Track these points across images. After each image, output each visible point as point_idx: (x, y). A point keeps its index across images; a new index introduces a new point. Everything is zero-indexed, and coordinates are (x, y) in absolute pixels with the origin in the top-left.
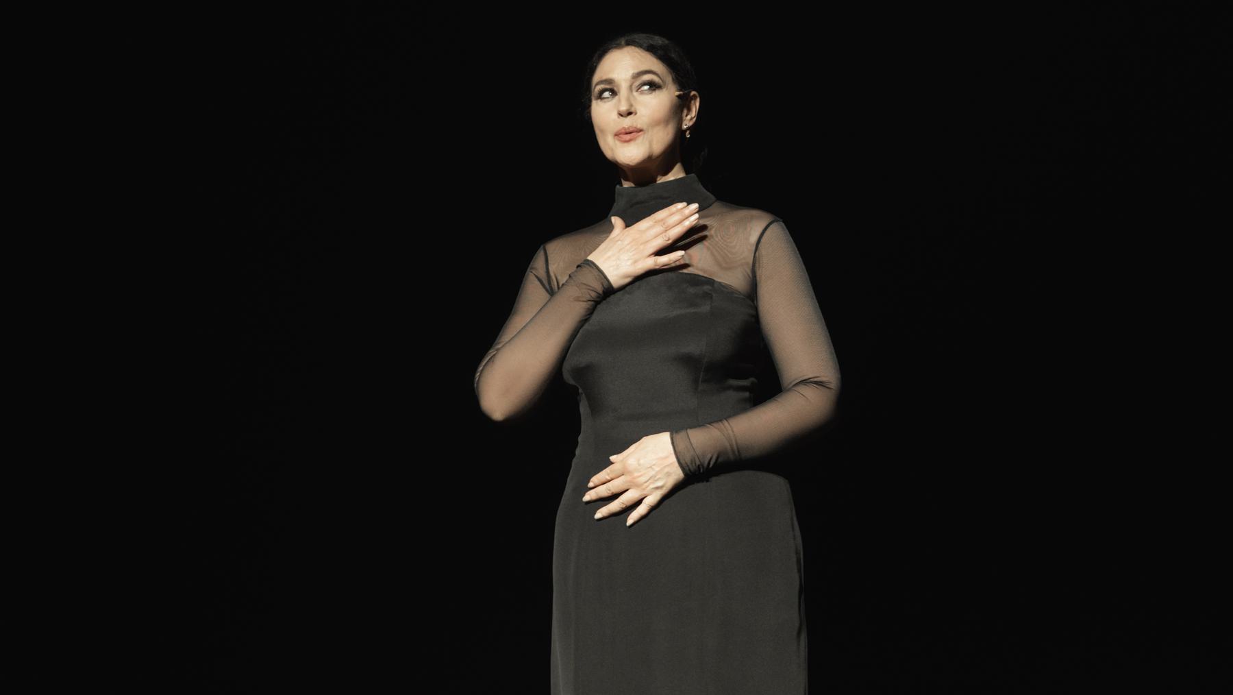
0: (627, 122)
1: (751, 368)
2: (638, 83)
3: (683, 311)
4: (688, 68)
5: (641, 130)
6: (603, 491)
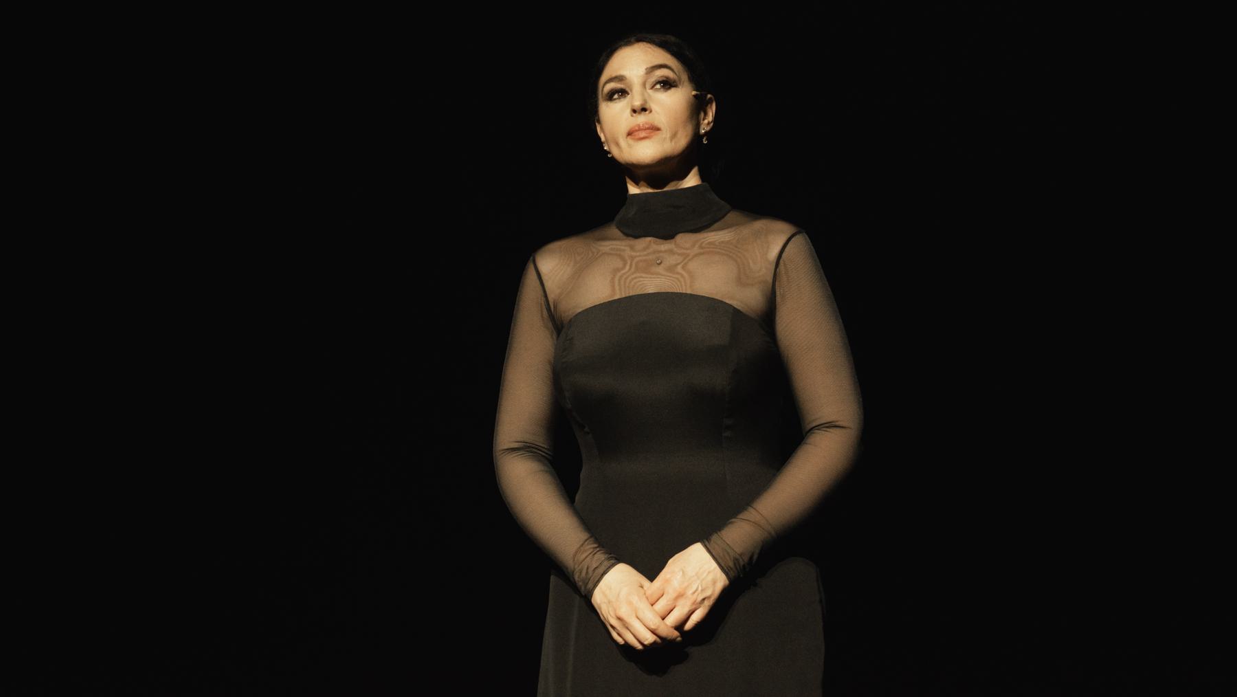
1: (766, 415)
2: (653, 79)
3: (650, 191)
4: (705, 69)
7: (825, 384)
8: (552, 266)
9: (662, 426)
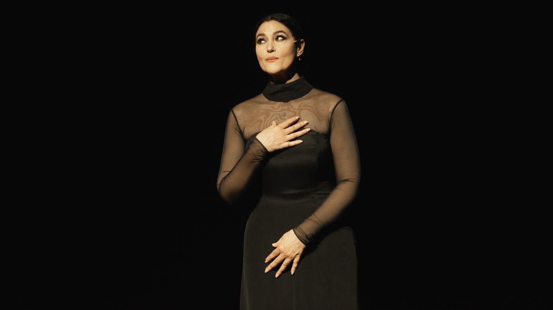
0: (271, 55)
5: (277, 58)
6: (273, 264)
7: (347, 163)
8: (241, 113)
9: (300, 174)
